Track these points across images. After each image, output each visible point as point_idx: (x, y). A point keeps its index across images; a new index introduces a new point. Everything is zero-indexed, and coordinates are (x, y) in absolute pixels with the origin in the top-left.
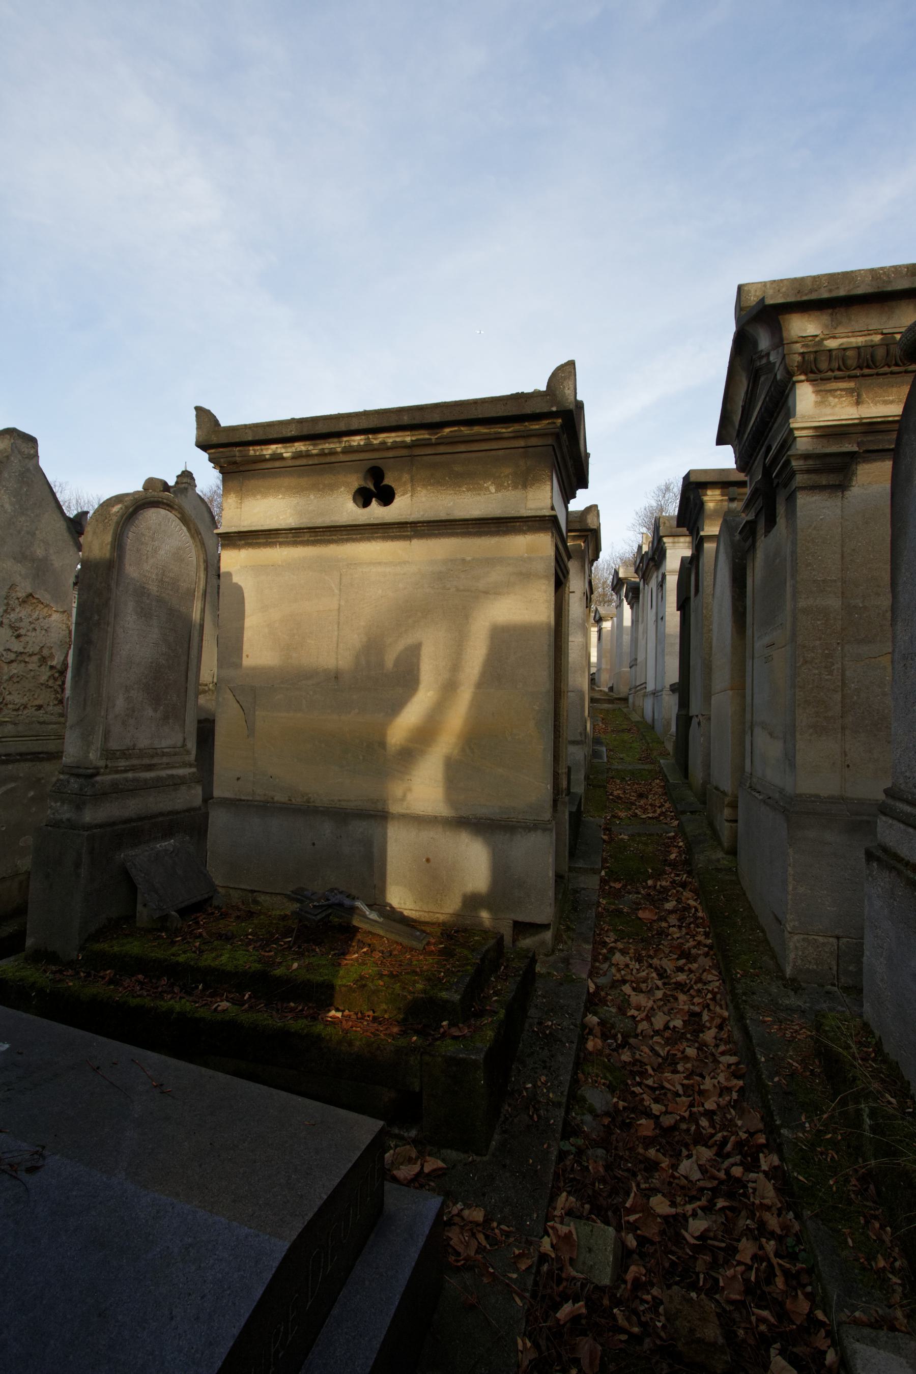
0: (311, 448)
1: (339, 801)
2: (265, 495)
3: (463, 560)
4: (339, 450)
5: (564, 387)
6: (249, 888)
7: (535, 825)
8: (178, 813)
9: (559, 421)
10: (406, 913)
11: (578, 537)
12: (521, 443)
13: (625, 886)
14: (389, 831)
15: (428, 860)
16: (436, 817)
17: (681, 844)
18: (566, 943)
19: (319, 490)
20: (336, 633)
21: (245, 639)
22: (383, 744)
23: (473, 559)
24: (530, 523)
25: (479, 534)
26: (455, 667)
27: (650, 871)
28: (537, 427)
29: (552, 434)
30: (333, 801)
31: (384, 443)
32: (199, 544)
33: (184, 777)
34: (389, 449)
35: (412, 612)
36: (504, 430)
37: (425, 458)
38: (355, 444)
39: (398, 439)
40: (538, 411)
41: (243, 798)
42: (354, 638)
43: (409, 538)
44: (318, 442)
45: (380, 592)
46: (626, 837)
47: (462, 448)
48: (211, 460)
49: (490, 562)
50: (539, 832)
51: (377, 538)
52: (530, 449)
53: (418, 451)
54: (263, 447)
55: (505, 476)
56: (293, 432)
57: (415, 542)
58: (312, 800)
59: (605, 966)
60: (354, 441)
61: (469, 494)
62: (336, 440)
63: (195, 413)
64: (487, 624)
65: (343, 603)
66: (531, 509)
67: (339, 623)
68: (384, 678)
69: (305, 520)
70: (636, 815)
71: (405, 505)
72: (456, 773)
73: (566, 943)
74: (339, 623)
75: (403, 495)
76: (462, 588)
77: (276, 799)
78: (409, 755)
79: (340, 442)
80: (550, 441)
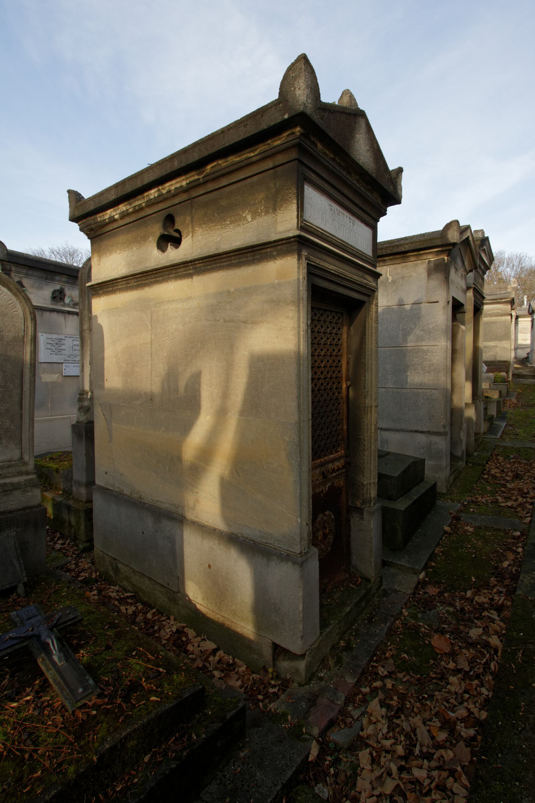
0: (128, 207)
1: (157, 501)
2: (111, 253)
3: (229, 291)
4: (144, 205)
5: (295, 89)
6: (114, 557)
7: (288, 555)
8: (11, 512)
9: (298, 130)
10: (198, 606)
11: (442, 252)
12: (269, 164)
13: (441, 593)
14: (184, 534)
15: (209, 566)
16: (215, 530)
17: (520, 550)
18: (329, 669)
19: (138, 243)
20: (150, 363)
21: (105, 367)
22: (180, 459)
23: (235, 290)
24: (279, 247)
25: (239, 265)
26: (225, 395)
27: (473, 579)
28: (279, 142)
29: (293, 146)
30: (153, 500)
31: (169, 191)
32: (23, 300)
33: (19, 484)
34: (174, 196)
35: (195, 343)
36: (252, 154)
37: (200, 198)
38: (152, 197)
39: (178, 185)
40: (272, 124)
41: (109, 488)
42: (161, 368)
43: (190, 276)
44: (131, 201)
45: (174, 326)
46: (471, 530)
47: (224, 182)
48: (81, 230)
49: (248, 291)
50: (290, 564)
51: (171, 277)
52: (278, 169)
53: (194, 193)
54: (104, 213)
55: (259, 202)
56: (113, 197)
57: (195, 278)
58: (142, 497)
59: (356, 713)
60: (151, 194)
61: (232, 226)
62: (140, 197)
63: (67, 195)
64: (247, 353)
65: (153, 337)
66: (280, 233)
67: (151, 353)
68: (178, 403)
69: (131, 269)
70: (497, 501)
71: (191, 246)
72: (229, 490)
73: (329, 669)
74: (151, 353)
75: (186, 237)
76: (227, 319)
77: (124, 491)
78: (197, 470)
79: (144, 198)
80: (294, 154)
